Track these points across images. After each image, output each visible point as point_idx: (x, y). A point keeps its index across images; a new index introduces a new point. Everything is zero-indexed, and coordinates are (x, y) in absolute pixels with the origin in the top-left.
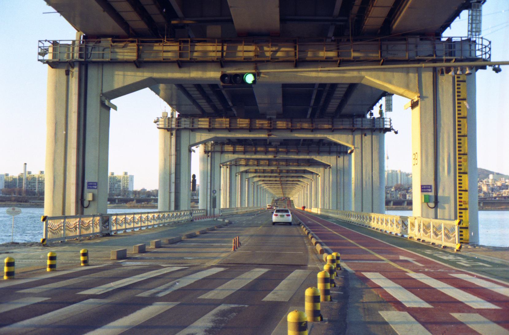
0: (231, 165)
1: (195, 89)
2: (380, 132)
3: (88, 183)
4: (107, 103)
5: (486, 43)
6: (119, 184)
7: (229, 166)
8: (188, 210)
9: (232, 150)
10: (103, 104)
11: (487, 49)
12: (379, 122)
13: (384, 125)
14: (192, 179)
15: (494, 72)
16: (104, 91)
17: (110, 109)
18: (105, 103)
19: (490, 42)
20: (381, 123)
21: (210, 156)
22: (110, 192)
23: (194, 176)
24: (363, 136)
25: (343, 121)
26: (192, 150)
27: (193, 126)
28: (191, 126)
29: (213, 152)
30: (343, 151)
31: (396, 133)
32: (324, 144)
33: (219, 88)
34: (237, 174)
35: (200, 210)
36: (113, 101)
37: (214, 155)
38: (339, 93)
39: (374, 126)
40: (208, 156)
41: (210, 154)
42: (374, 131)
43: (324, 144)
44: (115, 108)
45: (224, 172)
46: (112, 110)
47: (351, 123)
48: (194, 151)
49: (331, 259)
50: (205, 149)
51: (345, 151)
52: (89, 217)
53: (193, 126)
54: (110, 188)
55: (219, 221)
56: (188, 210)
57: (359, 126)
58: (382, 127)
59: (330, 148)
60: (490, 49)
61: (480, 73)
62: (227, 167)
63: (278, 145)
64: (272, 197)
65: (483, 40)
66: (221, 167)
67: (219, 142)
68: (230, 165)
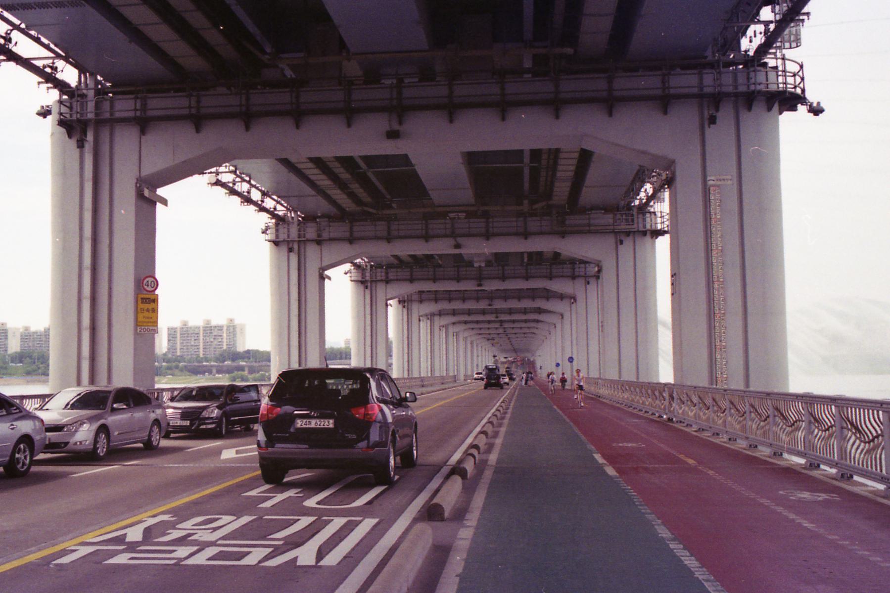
1: (310, 165)
2: (769, 109)
4: (147, 193)
5: (796, 68)
6: (220, 340)
7: (296, 246)
10: (140, 195)
11: (798, 80)
15: (812, 114)
16: (144, 174)
17: (156, 204)
18: (143, 194)
19: (801, 67)
21: (369, 287)
22: (204, 354)
24: (706, 126)
25: (563, 268)
26: (325, 276)
29: (303, 242)
30: (730, 89)
31: (816, 111)
32: (563, 262)
33: (362, 169)
34: (421, 318)
36: (161, 192)
37: (305, 248)
38: (566, 169)
41: (406, 304)
43: (563, 262)
44: (164, 202)
45: (393, 311)
46: (159, 206)
51: (742, 89)
54: (176, 337)
57: (582, 274)
60: (803, 79)
61: (786, 118)
65: (787, 62)
66: (420, 320)
68: (299, 242)
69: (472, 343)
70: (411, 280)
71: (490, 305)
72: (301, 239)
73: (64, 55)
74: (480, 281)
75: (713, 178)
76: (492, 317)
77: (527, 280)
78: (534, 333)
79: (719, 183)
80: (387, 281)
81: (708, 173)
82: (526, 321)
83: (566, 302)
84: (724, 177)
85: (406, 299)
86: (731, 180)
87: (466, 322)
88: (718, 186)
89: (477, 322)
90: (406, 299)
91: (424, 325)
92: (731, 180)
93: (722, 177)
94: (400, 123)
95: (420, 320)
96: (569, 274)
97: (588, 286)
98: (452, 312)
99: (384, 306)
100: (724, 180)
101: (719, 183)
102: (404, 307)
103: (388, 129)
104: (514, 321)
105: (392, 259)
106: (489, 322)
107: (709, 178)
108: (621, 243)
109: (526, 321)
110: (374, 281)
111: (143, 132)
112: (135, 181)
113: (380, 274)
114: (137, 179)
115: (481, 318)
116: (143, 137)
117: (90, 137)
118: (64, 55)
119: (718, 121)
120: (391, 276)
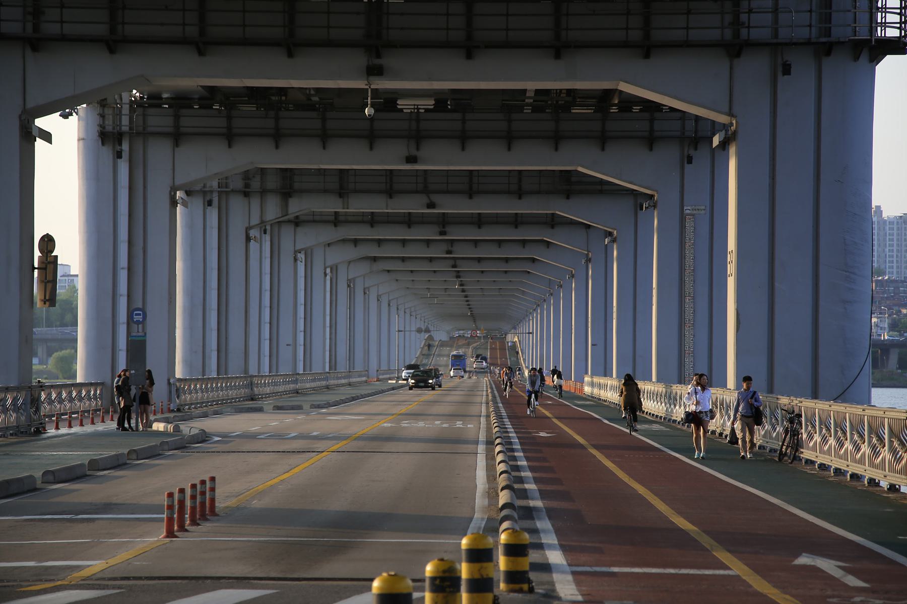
0: (227, 193)
2: (856, 58)
3: (73, 280)
8: (18, 389)
9: (170, 130)
12: (850, 15)
13: (872, 30)
14: (37, 254)
20: (864, 18)
21: (125, 155)
23: (48, 242)
24: (780, 74)
25: (689, 12)
27: (36, 28)
28: (29, 27)
34: (253, 233)
35: (81, 385)
39: (828, 33)
40: (119, 155)
42: (828, 53)
47: (728, 18)
48: (47, 137)
49: (471, 577)
50: (102, 126)
52: (404, 413)
53: (36, 28)
55: (460, 421)
56: (18, 389)
58: (863, 35)
59: (652, 120)
62: (210, 203)
63: (427, 110)
64: (419, 331)
66: (174, 203)
67: (165, 96)
68: (220, 193)
69: (350, 284)
70: (230, 137)
71: (411, 160)
72: (222, 190)
73: (828, 600)
74: (444, 227)
75: (689, 208)
76: (413, 205)
77: (558, 56)
78: (534, 260)
79: (695, 212)
80: (177, 137)
81: (685, 202)
82: (517, 221)
83: (669, 154)
84: (699, 208)
85: (125, 129)
86: (704, 210)
87: (336, 220)
88: (693, 215)
89: (373, 220)
90: (125, 129)
91: (261, 249)
92: (704, 210)
93: (697, 208)
94: (418, 149)
95: (248, 239)
96: (714, 35)
97: (687, 166)
98: (333, 218)
99: (323, 275)
100: (698, 210)
101: (695, 212)
102: (119, 155)
103: (407, 155)
104: (479, 221)
105: (200, 88)
106: (409, 221)
107: (685, 208)
108: (690, 161)
109: (517, 221)
110: (141, 134)
111: (177, 144)
112: (169, 189)
113: (160, 120)
114: (171, 188)
115: (376, 205)
116: (176, 149)
117: (125, 146)
118: (828, 600)
119: (792, 70)
120: (188, 122)
